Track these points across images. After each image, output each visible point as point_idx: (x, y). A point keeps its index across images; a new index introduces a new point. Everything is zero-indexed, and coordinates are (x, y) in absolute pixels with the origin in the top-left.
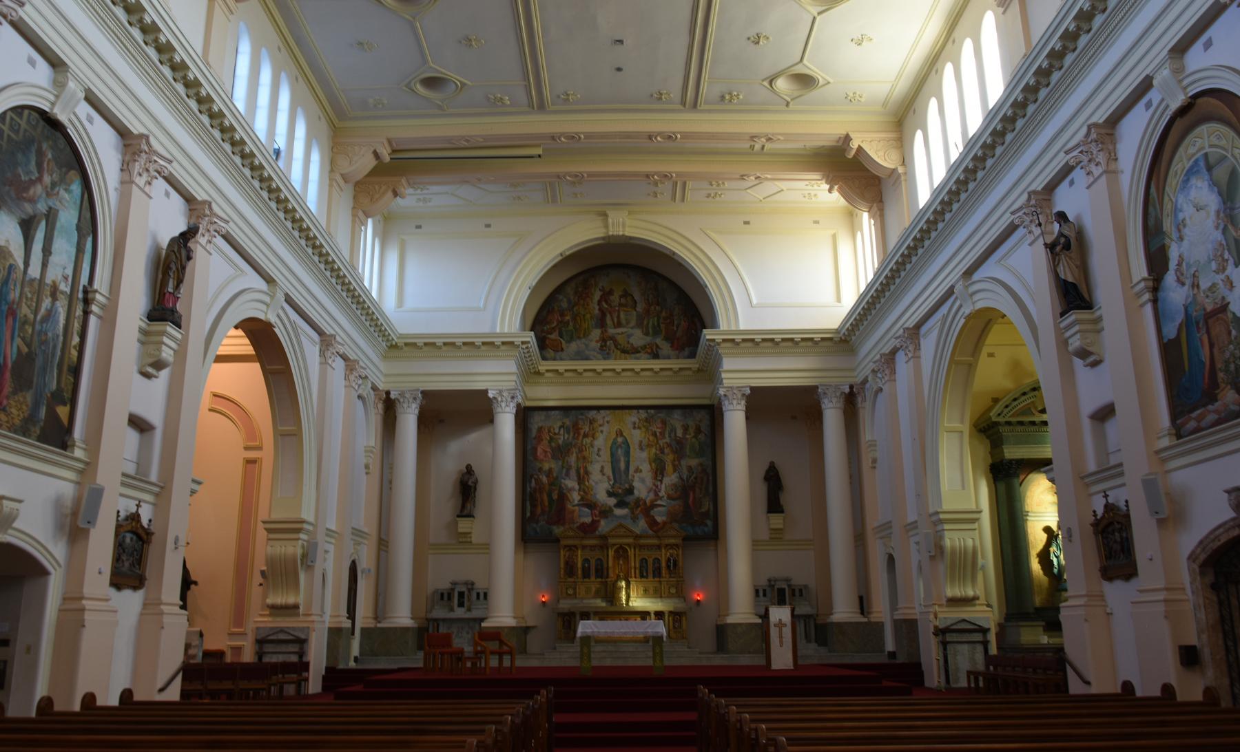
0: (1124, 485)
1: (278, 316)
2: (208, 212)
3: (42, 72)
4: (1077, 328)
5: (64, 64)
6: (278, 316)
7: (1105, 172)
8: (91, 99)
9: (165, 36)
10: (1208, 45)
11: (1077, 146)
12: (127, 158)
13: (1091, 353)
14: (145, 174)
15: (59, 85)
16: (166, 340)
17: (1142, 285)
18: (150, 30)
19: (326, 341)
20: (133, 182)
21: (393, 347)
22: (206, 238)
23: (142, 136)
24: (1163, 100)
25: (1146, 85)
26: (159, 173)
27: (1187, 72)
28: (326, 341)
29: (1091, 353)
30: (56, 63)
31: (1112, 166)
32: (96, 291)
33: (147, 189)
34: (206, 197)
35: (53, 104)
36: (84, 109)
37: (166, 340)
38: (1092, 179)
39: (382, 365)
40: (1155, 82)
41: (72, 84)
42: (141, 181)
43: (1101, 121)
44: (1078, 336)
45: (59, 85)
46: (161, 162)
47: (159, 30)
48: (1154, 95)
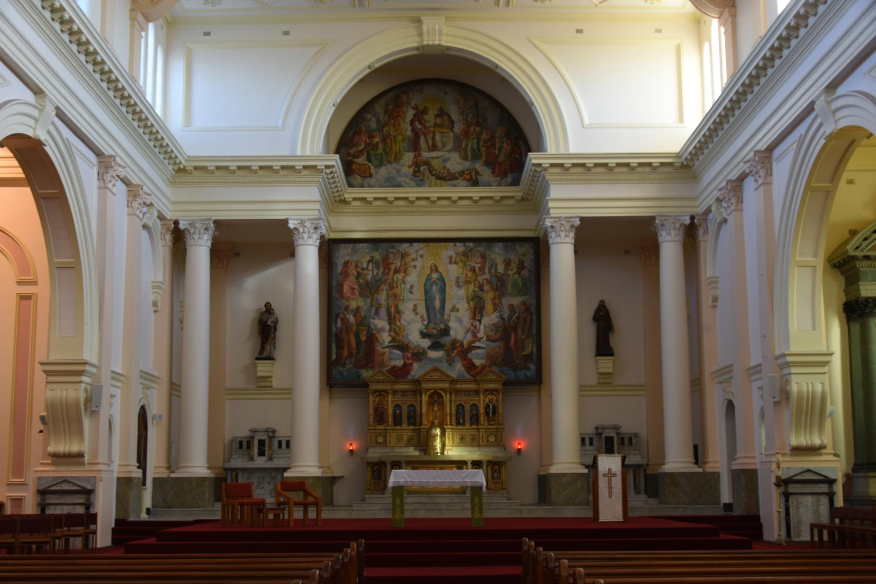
1: (49, 132)
6: (49, 132)
19: (105, 162)
20: (108, 188)
23: (111, 156)
30: (37, 91)
31: (768, 180)
34: (139, 182)
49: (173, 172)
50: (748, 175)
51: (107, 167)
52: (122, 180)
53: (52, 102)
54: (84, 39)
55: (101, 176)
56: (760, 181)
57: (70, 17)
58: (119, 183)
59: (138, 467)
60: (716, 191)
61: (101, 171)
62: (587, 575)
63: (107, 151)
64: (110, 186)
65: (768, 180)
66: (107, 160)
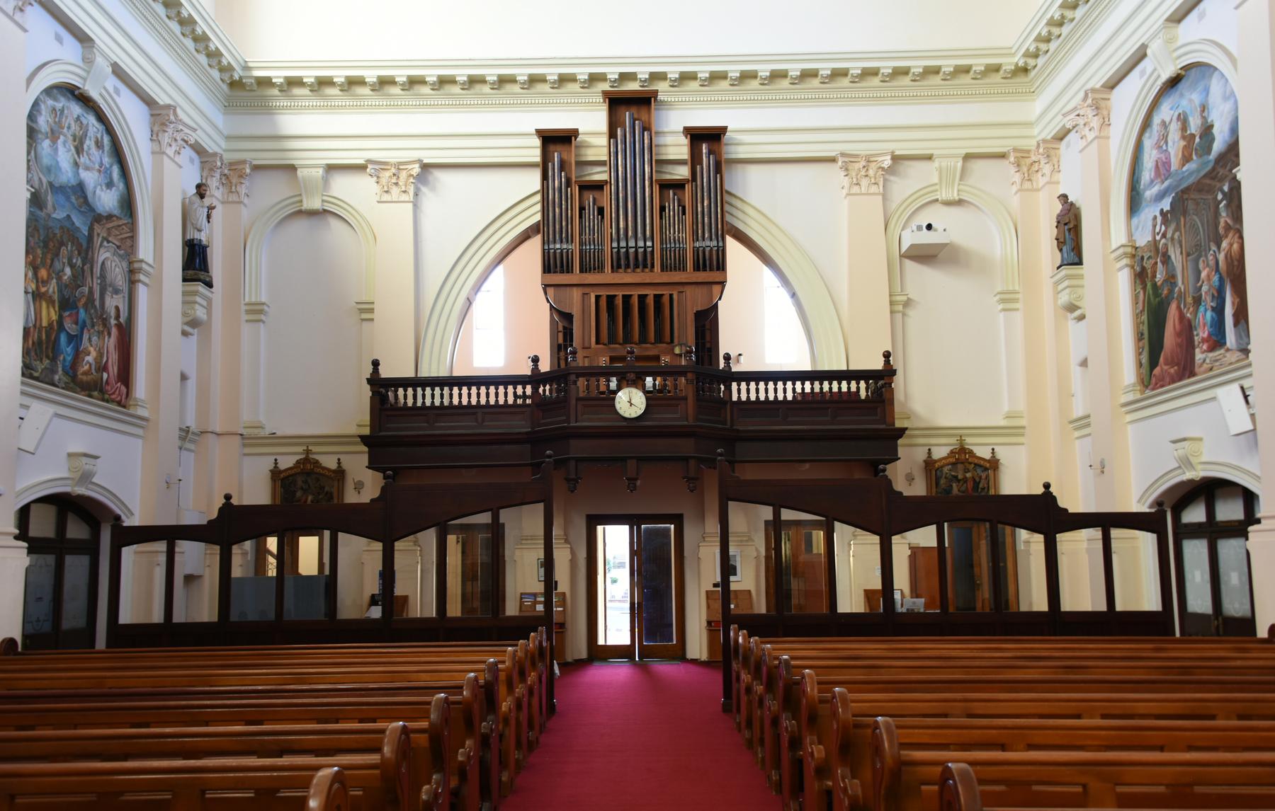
0: (1250, 375)
1: (101, 95)
2: (172, 118)
3: (70, 50)
4: (1066, 283)
5: (91, 40)
6: (101, 95)
7: (1096, 137)
8: (118, 72)
9: (215, 43)
10: (1201, 17)
11: (1075, 109)
12: (156, 129)
13: (1079, 308)
14: (174, 144)
15: (88, 61)
16: (198, 299)
17: (1121, 251)
18: (187, 23)
19: (160, 115)
20: (164, 153)
21: (236, 85)
22: (174, 148)
23: (168, 107)
24: (1155, 69)
25: (1140, 56)
26: (186, 142)
27: (1179, 43)
28: (160, 115)
29: (1079, 308)
30: (83, 38)
31: (1055, 178)
32: (142, 261)
33: (18, 16)
34: (168, 101)
35: (85, 79)
36: (112, 82)
37: (198, 299)
38: (1084, 143)
39: (219, 119)
40: (1149, 52)
41: (99, 60)
42: (170, 151)
43: (1098, 86)
44: (1067, 291)
45: (88, 61)
46: (186, 131)
47: (209, 39)
48: (1146, 65)
49: (225, 87)
50: (1069, 131)
51: (163, 124)
52: (192, 146)
53: (106, 57)
54: (225, 62)
55: (154, 137)
56: (1091, 136)
57: (204, 32)
58: (188, 152)
59: (17, 538)
60: (1060, 117)
61: (156, 129)
62: (793, 658)
63: (162, 99)
64: (170, 151)
65: (1055, 178)
66: (163, 112)
